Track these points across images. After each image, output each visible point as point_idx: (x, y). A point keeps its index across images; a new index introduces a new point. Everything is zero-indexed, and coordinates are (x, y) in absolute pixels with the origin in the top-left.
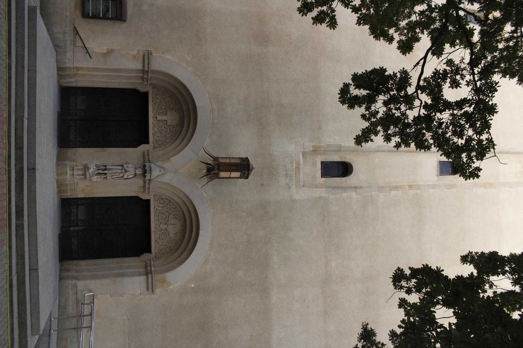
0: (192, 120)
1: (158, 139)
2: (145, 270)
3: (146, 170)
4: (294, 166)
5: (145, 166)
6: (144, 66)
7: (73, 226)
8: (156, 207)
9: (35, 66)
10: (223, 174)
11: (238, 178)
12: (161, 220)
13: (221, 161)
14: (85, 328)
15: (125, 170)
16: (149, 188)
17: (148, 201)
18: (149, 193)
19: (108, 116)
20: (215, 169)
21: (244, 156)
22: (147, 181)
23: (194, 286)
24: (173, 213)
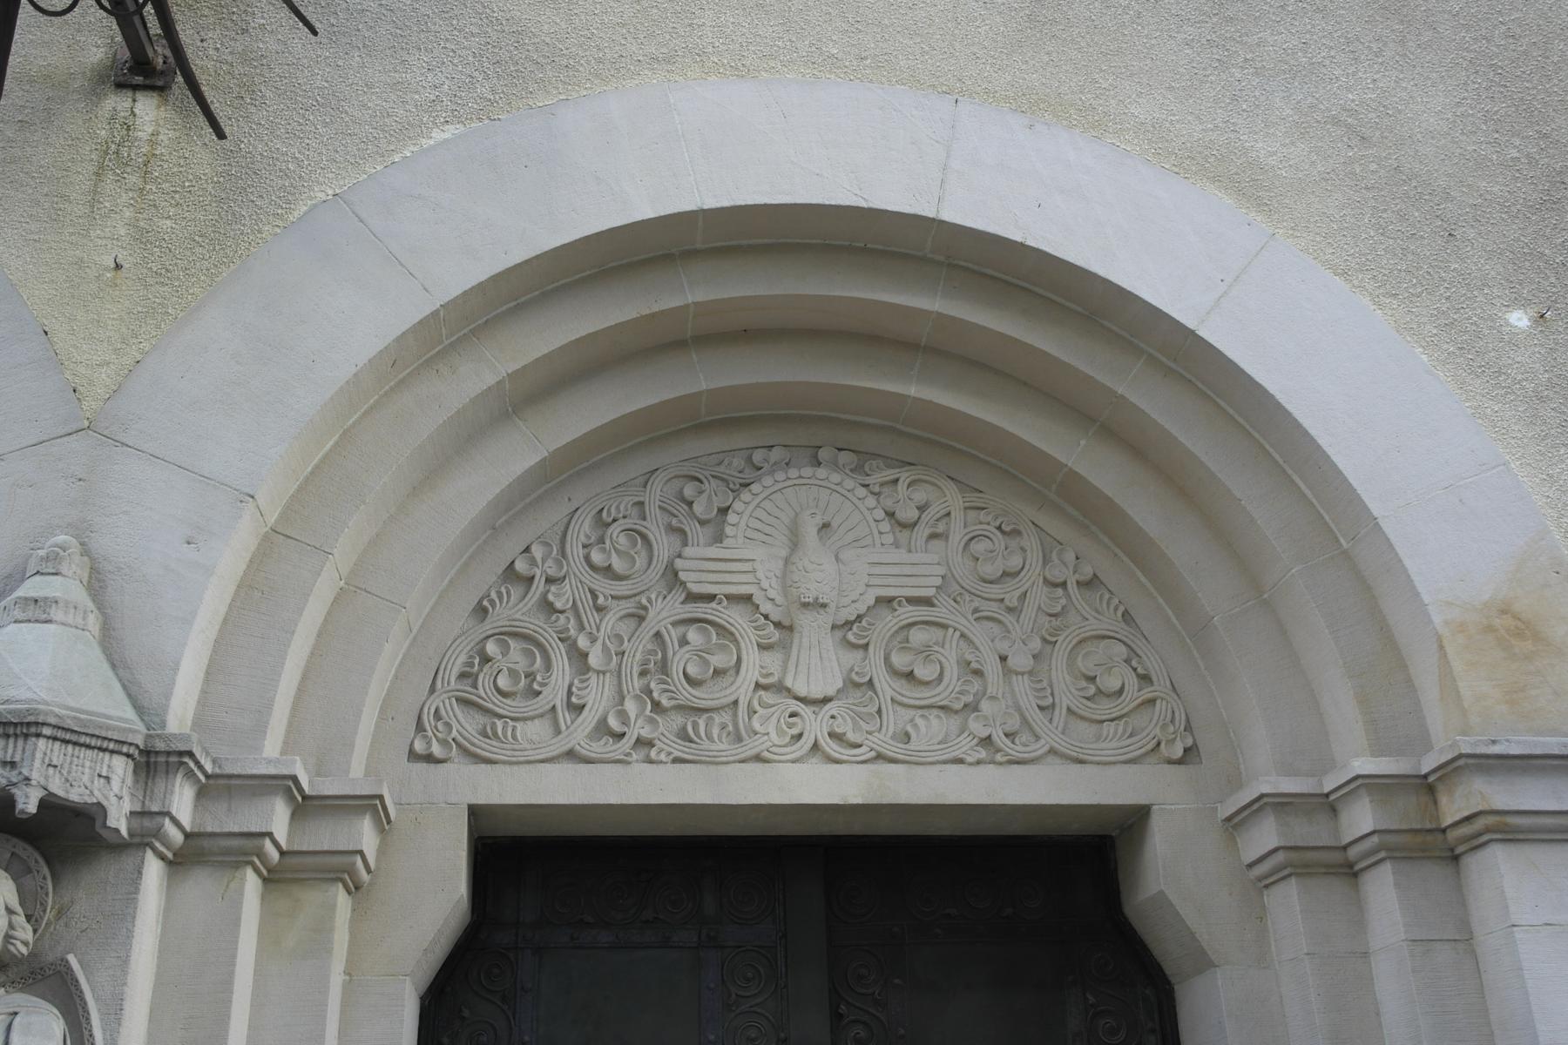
4: (450, 131)
8: (579, 733)
12: (742, 688)
23: (1518, 302)
24: (664, 547)
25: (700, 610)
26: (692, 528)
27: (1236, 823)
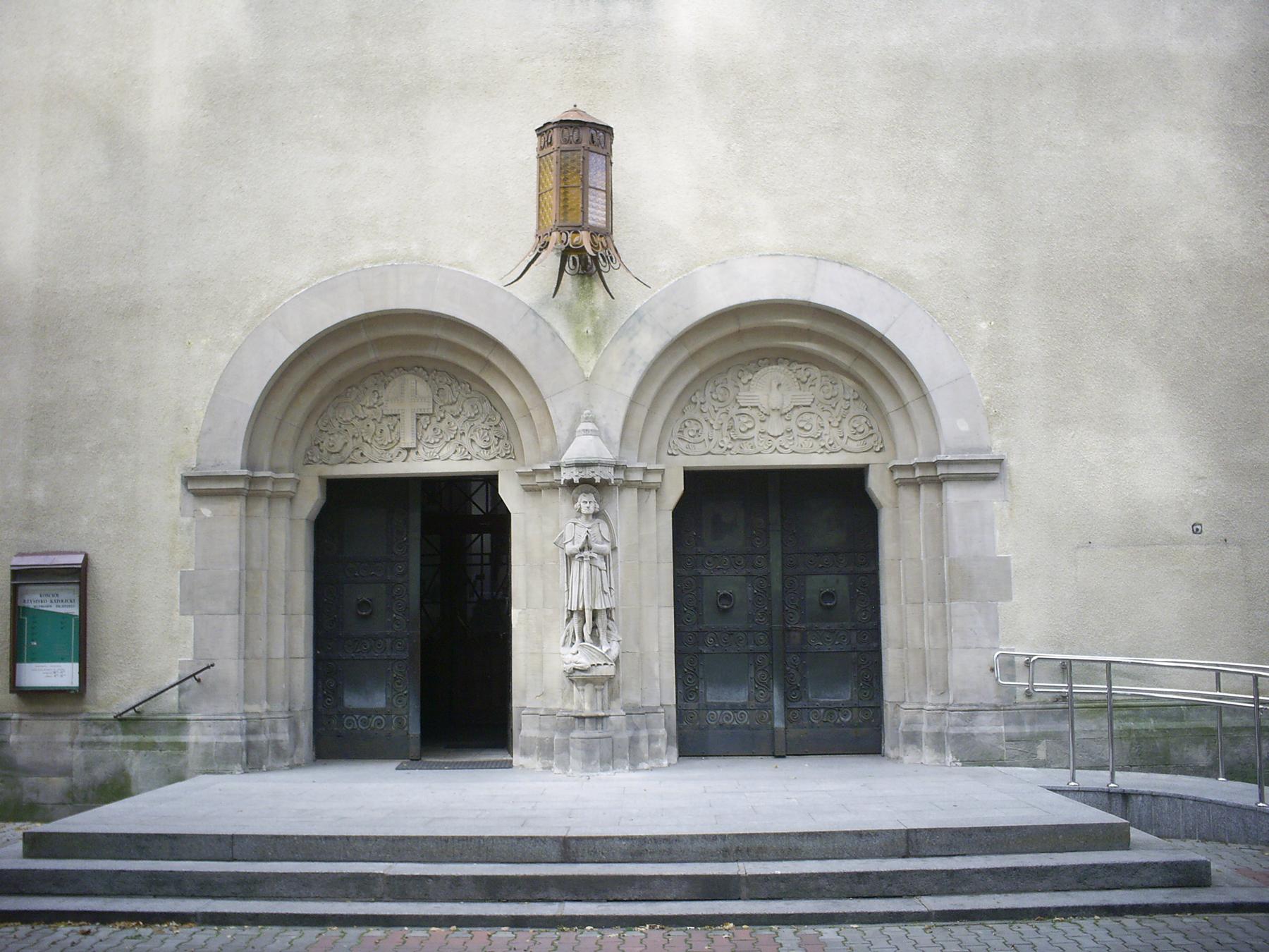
0: (414, 330)
1: (480, 442)
2: (922, 487)
3: (583, 481)
5: (570, 485)
6: (235, 493)
7: (771, 718)
9: (220, 838)
10: (596, 217)
11: (609, 163)
13: (550, 222)
14: (1110, 684)
15: (582, 550)
16: (646, 471)
17: (692, 477)
18: (662, 472)
19: (412, 614)
20: (585, 259)
21: (534, 141)
22: (621, 476)
25: (743, 411)
26: (741, 386)
27: (893, 469)
